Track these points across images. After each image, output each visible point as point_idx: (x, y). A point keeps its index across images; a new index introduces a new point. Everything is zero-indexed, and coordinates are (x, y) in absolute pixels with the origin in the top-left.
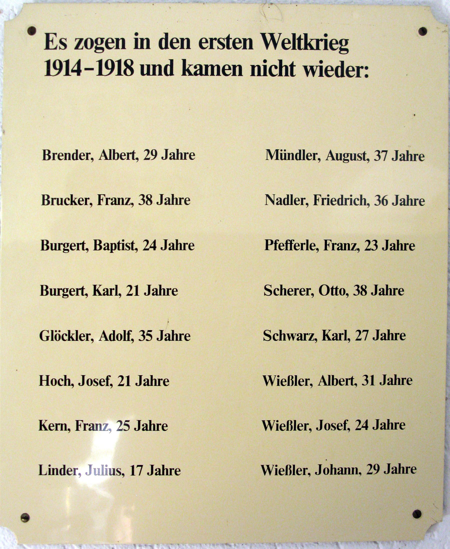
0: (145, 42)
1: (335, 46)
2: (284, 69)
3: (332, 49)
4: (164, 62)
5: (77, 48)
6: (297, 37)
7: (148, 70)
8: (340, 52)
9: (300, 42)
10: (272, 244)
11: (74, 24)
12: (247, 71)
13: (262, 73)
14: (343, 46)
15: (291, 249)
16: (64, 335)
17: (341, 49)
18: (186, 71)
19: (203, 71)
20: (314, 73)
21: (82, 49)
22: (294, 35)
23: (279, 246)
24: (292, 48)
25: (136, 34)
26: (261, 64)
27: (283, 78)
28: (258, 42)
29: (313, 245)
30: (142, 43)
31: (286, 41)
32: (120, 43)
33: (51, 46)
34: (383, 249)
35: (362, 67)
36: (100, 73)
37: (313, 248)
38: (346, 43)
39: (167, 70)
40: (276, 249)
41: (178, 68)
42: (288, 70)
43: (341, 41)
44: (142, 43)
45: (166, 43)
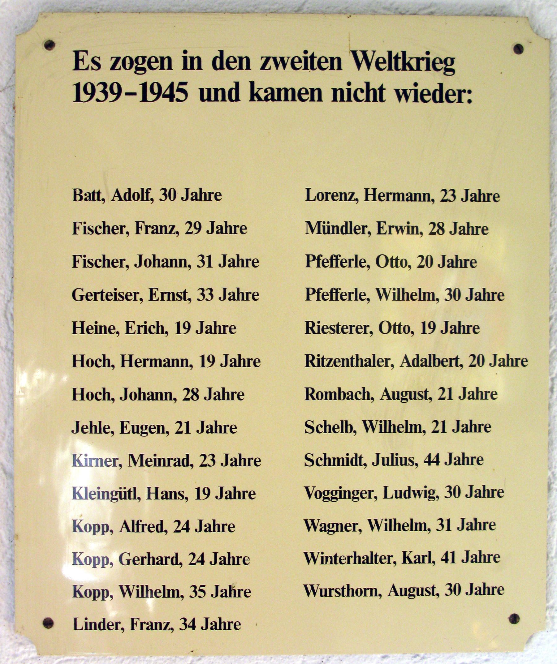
0: (196, 61)
1: (438, 66)
2: (371, 93)
3: (436, 69)
4: (228, 85)
5: (113, 68)
6: (394, 55)
7: (208, 95)
8: (444, 74)
9: (397, 62)
10: (314, 293)
11: (111, 39)
12: (327, 95)
13: (346, 98)
14: (448, 66)
15: (337, 299)
16: (98, 360)
17: (446, 70)
18: (254, 96)
19: (275, 95)
20: (407, 98)
21: (120, 69)
22: (390, 53)
23: (323, 296)
24: (387, 68)
25: (185, 52)
26: (345, 87)
27: (371, 104)
28: (348, 62)
29: (362, 294)
30: (192, 63)
31: (381, 60)
32: (165, 63)
33: (81, 66)
34: (211, 563)
35: (464, 91)
36: (145, 99)
37: (363, 298)
38: (452, 63)
39: (232, 95)
40: (318, 299)
41: (245, 92)
42: (376, 95)
43: (446, 60)
44: (192, 63)
45: (221, 62)
